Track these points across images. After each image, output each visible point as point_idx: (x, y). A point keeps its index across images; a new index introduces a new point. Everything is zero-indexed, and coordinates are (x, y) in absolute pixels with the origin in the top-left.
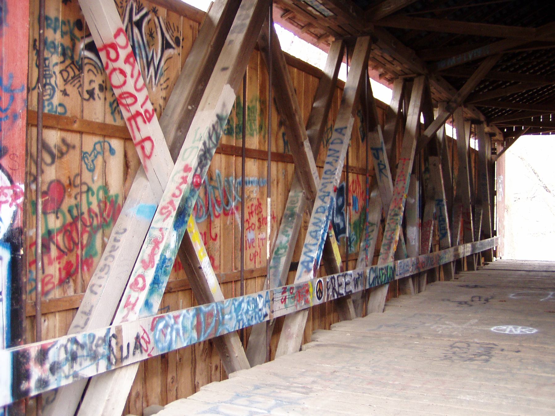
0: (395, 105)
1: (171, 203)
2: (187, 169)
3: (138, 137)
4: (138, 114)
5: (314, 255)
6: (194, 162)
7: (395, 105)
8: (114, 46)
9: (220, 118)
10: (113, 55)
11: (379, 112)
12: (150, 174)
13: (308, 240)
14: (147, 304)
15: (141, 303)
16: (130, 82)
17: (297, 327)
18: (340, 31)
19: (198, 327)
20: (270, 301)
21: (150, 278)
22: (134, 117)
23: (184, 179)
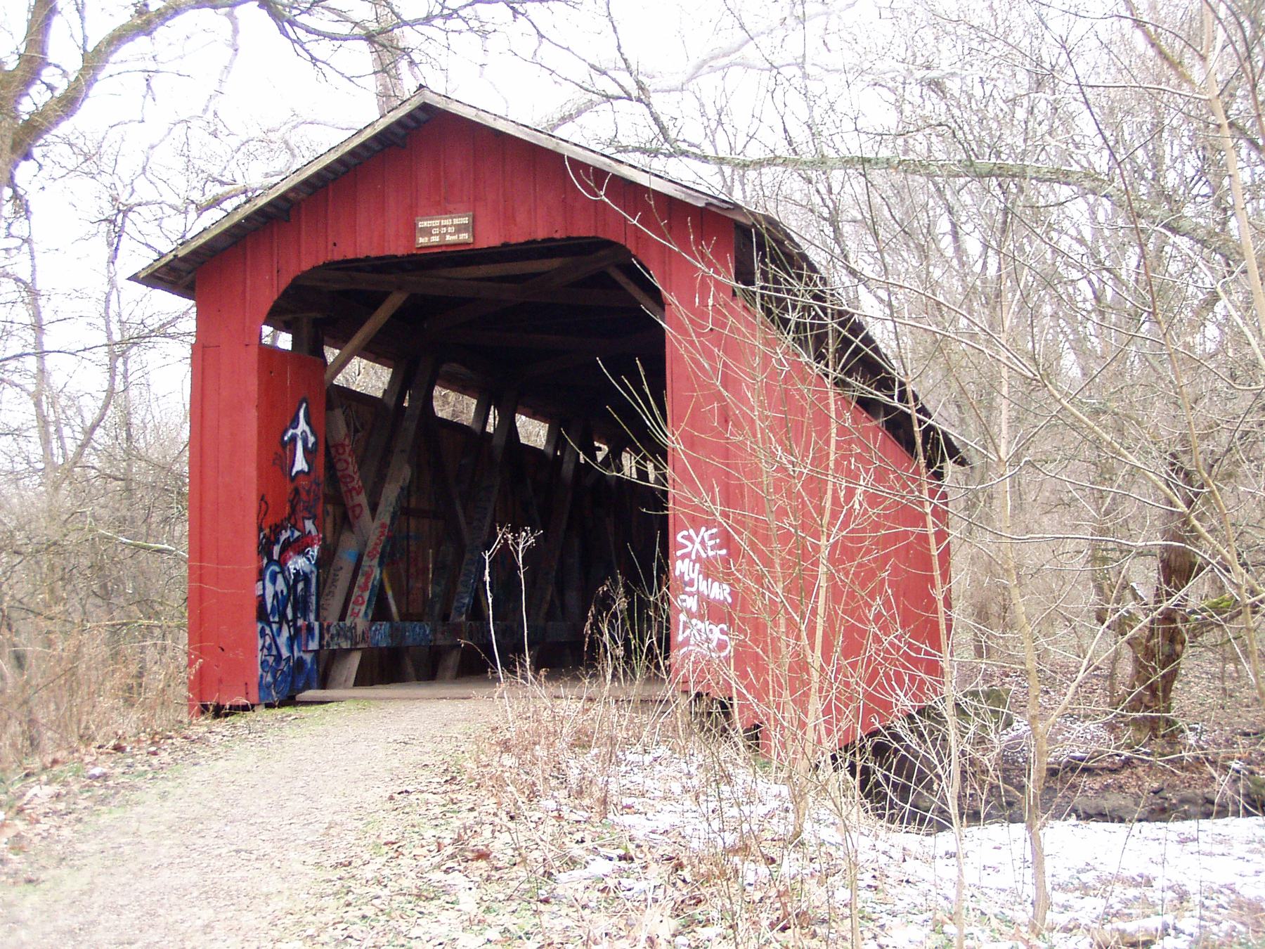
0: (521, 420)
1: (375, 549)
2: (383, 526)
3: (351, 504)
4: (354, 488)
5: (466, 601)
6: (387, 521)
7: (521, 420)
8: (343, 445)
9: (402, 488)
10: (341, 451)
11: (292, 195)
12: (356, 529)
13: (460, 588)
14: (366, 613)
15: (362, 614)
16: (351, 468)
17: (453, 660)
18: (640, 664)
19: (391, 636)
20: (434, 631)
21: (366, 598)
22: (350, 491)
23: (383, 534)
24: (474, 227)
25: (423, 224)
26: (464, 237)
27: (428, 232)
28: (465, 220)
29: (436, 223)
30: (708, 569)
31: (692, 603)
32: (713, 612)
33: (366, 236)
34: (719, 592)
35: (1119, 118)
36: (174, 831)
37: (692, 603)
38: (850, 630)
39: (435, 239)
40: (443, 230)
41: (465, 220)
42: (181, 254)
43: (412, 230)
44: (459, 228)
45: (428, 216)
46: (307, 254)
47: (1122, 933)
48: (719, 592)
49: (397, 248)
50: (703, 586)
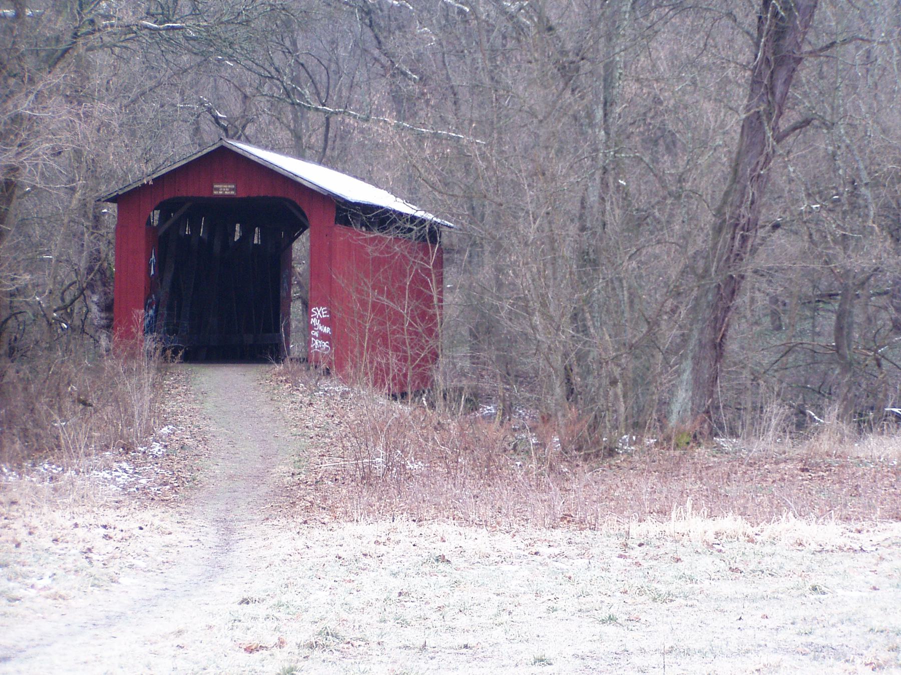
24: (235, 190)
25: (216, 186)
26: (233, 193)
27: (218, 189)
28: (233, 186)
29: (220, 186)
30: (323, 322)
31: (316, 334)
32: (323, 337)
33: (190, 190)
34: (327, 330)
35: (368, 100)
36: (740, 362)
37: (316, 334)
38: (373, 346)
39: (221, 192)
40: (224, 189)
41: (233, 186)
42: (120, 193)
43: (212, 189)
44: (230, 190)
45: (218, 183)
46: (167, 194)
47: (684, 371)
48: (327, 330)
49: (205, 194)
50: (320, 328)
